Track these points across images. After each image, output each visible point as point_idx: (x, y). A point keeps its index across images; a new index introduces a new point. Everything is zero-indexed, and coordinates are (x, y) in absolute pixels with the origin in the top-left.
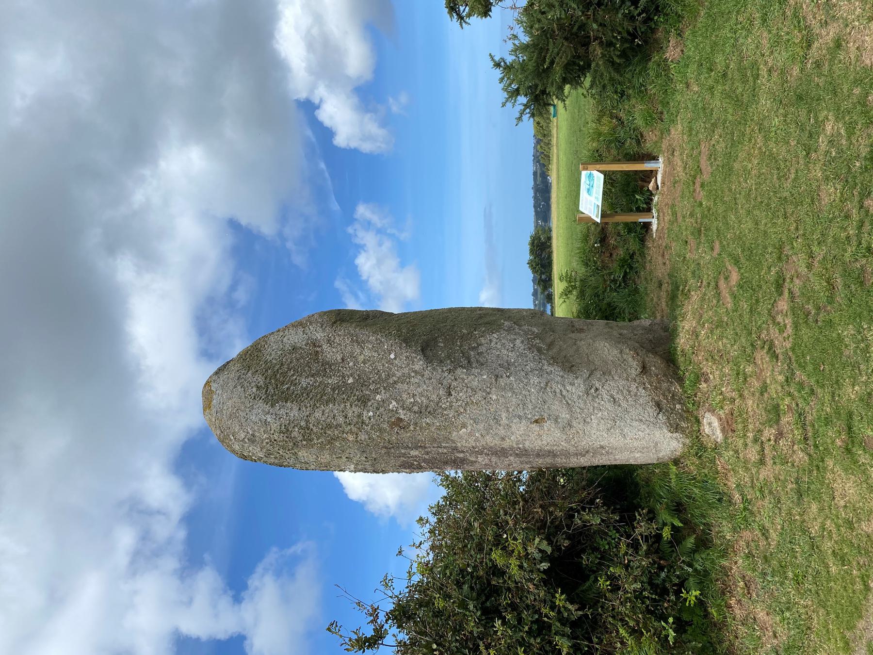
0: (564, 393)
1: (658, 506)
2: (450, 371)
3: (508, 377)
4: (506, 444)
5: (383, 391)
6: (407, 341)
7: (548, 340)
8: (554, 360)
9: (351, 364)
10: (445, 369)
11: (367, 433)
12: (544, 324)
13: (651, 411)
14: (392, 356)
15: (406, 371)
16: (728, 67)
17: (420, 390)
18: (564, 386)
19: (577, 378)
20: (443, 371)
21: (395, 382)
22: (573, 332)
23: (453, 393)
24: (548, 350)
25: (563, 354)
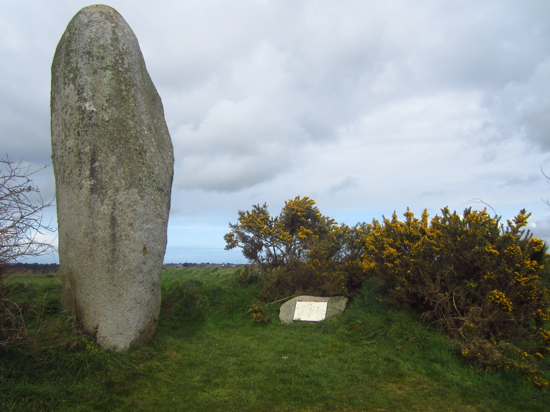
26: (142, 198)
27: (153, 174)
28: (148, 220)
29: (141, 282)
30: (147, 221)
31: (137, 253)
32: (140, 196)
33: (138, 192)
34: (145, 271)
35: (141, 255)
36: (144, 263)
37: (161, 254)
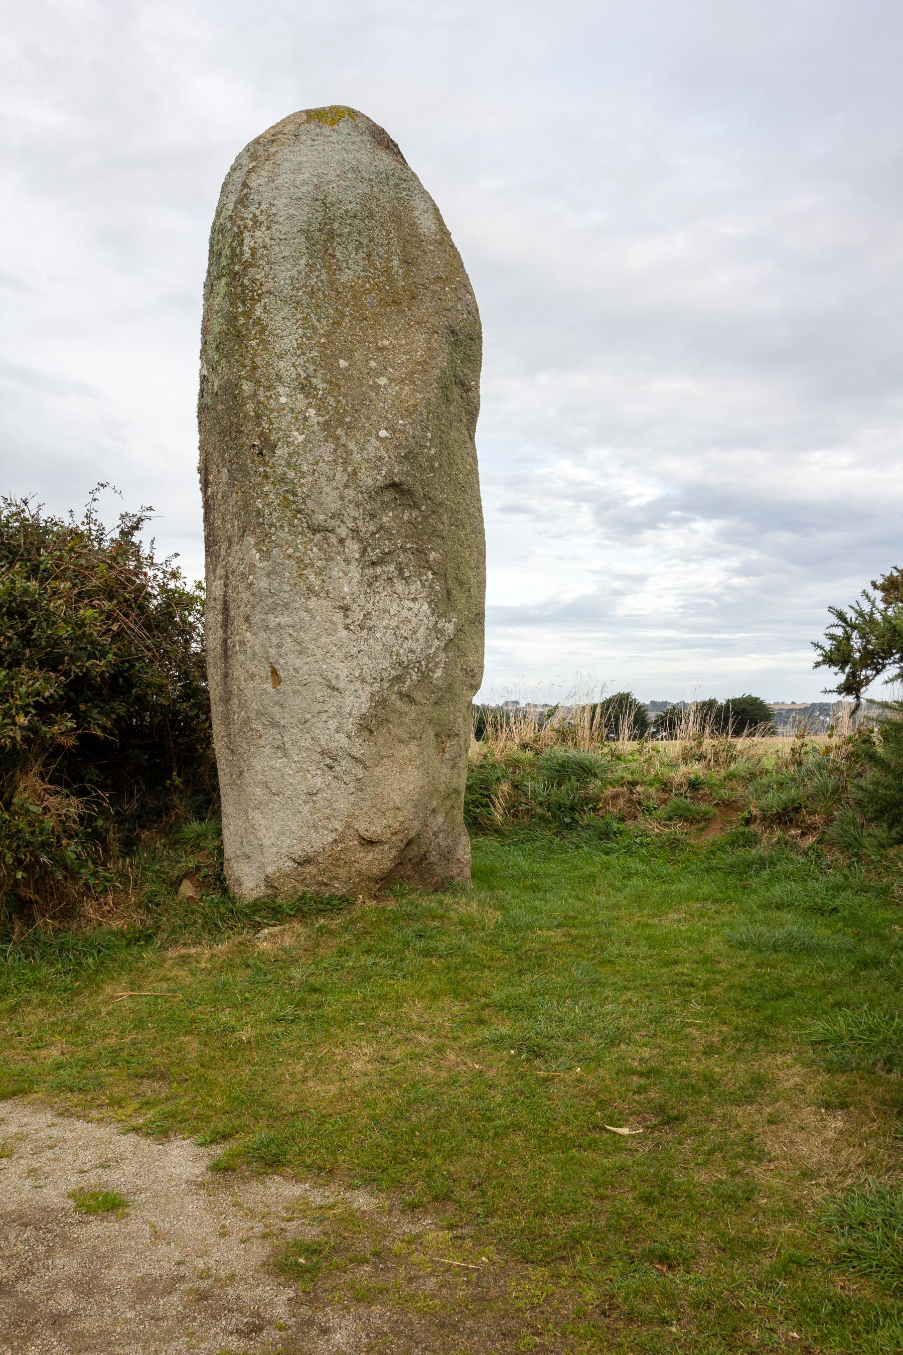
0: (324, 716)
1: (73, 807)
2: (355, 531)
3: (347, 628)
4: (238, 623)
5: (322, 419)
7: (418, 695)
8: (380, 702)
9: (373, 364)
10: (360, 523)
12: (450, 688)
13: (298, 852)
14: (383, 433)
15: (357, 457)
19: (349, 737)
20: (355, 519)
22: (437, 735)
23: (318, 536)
24: (400, 693)
25: (393, 717)
29: (278, 748)
33: (257, 544)
37: (473, 682)
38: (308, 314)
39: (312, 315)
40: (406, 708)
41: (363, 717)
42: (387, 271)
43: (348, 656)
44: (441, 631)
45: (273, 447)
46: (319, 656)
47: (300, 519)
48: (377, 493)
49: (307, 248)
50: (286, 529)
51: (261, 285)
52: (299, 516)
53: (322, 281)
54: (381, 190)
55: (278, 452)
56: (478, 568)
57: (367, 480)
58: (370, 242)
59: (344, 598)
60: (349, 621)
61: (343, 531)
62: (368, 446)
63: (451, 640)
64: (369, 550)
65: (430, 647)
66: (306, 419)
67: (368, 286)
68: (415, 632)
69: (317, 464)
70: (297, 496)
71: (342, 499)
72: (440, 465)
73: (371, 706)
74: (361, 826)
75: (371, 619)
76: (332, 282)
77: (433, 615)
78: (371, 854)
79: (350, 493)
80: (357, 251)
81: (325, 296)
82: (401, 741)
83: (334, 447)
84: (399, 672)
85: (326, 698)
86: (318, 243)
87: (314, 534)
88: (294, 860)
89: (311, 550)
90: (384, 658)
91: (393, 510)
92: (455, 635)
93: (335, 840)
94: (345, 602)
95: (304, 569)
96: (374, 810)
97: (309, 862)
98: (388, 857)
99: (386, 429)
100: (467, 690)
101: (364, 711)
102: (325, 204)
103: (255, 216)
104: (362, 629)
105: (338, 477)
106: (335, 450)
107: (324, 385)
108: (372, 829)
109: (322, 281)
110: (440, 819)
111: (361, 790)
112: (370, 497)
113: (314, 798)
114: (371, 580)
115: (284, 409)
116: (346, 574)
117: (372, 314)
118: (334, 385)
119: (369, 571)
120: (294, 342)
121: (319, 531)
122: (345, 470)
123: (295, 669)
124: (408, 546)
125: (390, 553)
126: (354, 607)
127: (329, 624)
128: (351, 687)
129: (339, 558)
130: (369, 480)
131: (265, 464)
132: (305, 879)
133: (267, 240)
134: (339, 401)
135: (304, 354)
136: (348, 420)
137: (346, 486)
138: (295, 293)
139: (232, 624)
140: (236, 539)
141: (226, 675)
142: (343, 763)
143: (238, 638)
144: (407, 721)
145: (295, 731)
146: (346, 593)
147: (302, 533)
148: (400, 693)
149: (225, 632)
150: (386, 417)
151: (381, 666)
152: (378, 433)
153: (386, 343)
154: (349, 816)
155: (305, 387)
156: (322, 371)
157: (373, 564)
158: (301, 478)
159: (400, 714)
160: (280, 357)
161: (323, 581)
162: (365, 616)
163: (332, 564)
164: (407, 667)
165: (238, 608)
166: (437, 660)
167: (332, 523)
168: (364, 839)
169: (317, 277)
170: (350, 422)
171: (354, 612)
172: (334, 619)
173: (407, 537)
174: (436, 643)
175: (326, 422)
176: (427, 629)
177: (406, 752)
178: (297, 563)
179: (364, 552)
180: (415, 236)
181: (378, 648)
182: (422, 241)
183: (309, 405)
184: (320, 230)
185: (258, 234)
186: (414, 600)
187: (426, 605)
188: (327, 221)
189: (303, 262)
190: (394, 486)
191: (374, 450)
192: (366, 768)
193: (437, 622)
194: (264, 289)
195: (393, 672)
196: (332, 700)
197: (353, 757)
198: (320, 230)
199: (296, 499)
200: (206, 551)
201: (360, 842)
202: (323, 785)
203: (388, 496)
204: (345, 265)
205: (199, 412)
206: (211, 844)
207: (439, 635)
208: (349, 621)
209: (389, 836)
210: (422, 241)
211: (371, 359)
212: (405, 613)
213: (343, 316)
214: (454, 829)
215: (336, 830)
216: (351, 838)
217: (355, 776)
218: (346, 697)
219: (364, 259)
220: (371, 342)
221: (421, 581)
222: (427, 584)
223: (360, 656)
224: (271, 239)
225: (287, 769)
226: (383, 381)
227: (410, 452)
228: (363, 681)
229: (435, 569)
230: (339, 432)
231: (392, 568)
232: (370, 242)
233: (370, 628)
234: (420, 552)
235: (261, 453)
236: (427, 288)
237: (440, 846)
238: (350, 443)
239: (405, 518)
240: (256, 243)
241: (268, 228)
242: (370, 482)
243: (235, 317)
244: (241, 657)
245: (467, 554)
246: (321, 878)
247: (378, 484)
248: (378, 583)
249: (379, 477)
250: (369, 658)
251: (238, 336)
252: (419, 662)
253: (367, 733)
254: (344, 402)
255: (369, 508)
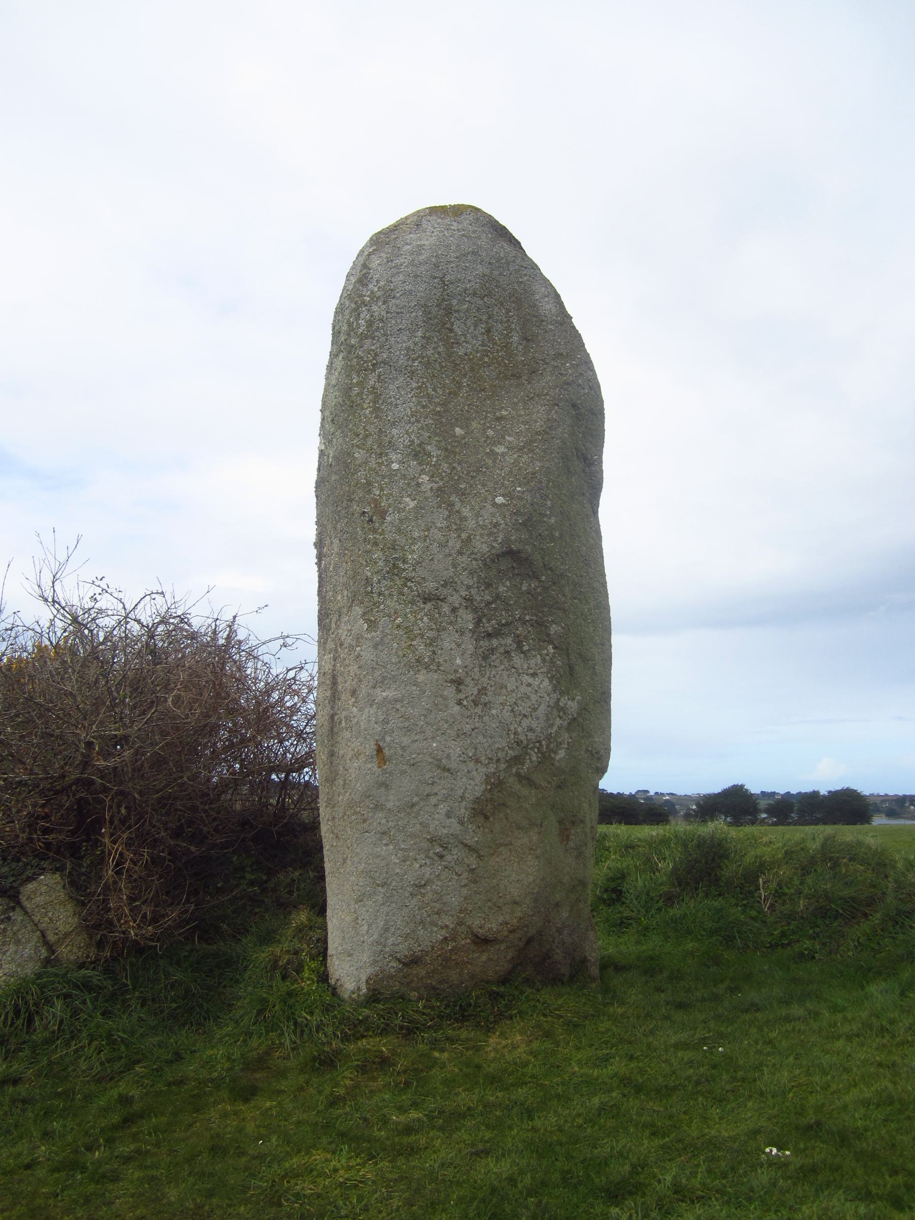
0: (433, 800)
2: (469, 600)
3: (459, 703)
5: (435, 486)
6: (529, 523)
8: (495, 784)
9: (490, 432)
10: (473, 591)
11: (366, 463)
13: (403, 950)
15: (471, 524)
16: (703, 1000)
17: (435, 548)
18: (446, 799)
19: (461, 823)
20: (469, 587)
21: (451, 505)
22: (560, 822)
23: (429, 606)
24: (518, 775)
26: (372, 625)
27: (404, 562)
28: (384, 678)
29: (383, 833)
30: (382, 682)
31: (362, 758)
32: (368, 621)
33: (364, 614)
34: (389, 805)
35: (373, 766)
36: (384, 785)
37: (599, 761)
38: (423, 383)
39: (428, 384)
40: (525, 791)
41: (477, 801)
42: (507, 346)
43: (461, 734)
44: (563, 710)
45: (383, 514)
46: (429, 734)
47: (410, 587)
48: (493, 561)
49: (424, 322)
50: (395, 598)
51: (376, 355)
52: (409, 584)
53: (439, 353)
54: (501, 274)
55: (388, 519)
56: (603, 645)
57: (481, 546)
58: (489, 318)
59: (456, 671)
60: (462, 696)
61: (455, 600)
62: (483, 512)
63: (574, 719)
64: (484, 620)
65: (551, 726)
66: (418, 485)
67: (486, 360)
68: (535, 710)
69: (428, 530)
70: (407, 563)
71: (455, 566)
72: (561, 535)
73: (486, 790)
74: (475, 922)
75: (486, 694)
76: (450, 355)
77: (555, 691)
78: (486, 954)
79: (464, 560)
80: (476, 326)
81: (442, 367)
82: (519, 828)
83: (447, 513)
84: (517, 753)
85: (436, 780)
86: (435, 317)
87: (424, 603)
88: (399, 960)
89: (421, 619)
90: (501, 737)
91: (509, 579)
92: (578, 714)
93: (446, 939)
94: (458, 675)
95: (412, 640)
96: (489, 904)
97: (416, 963)
98: (505, 957)
99: (503, 496)
100: (592, 773)
101: (478, 794)
102: (443, 282)
103: (372, 292)
104: (476, 705)
105: (450, 544)
106: (449, 516)
107: (439, 452)
108: (488, 926)
109: (439, 353)
110: (565, 914)
111: (475, 882)
112: (485, 564)
113: (422, 891)
114: (486, 652)
115: (396, 475)
116: (459, 646)
117: (491, 386)
118: (448, 453)
119: (485, 643)
120: (408, 410)
121: (430, 600)
122: (459, 536)
123: (403, 748)
124: (527, 618)
125: (507, 624)
126: (468, 680)
127: (440, 699)
128: (464, 768)
129: (451, 628)
130: (484, 546)
131: (375, 531)
132: (412, 981)
133: (383, 313)
134: (454, 468)
135: (418, 421)
136: (463, 486)
137: (460, 553)
138: (410, 363)
139: (339, 699)
140: (345, 610)
141: (332, 754)
142: (454, 852)
143: (344, 713)
144: (527, 806)
145: (402, 815)
146: (458, 666)
147: (413, 603)
148: (518, 775)
149: (332, 708)
150: (503, 484)
151: (497, 746)
152: (494, 499)
153: (504, 413)
154: (461, 911)
155: (418, 453)
156: (437, 438)
157: (489, 636)
158: (412, 544)
159: (519, 798)
160: (394, 424)
161: (434, 653)
162: (479, 691)
163: (444, 635)
164: (526, 747)
165: (346, 682)
166: (560, 740)
167: (445, 592)
168: (477, 937)
169: (434, 348)
170: (465, 489)
171: (467, 686)
172: (445, 693)
173: (525, 608)
174: (558, 722)
175: (439, 489)
176: (548, 706)
177: (526, 840)
178: (406, 633)
179: (478, 622)
180: (535, 316)
181: (494, 726)
182: (543, 321)
183: (423, 472)
184: (438, 306)
185: (375, 308)
186: (534, 675)
187: (547, 680)
188: (446, 297)
189: (420, 334)
190: (510, 553)
191: (487, 516)
192: (480, 857)
193: (558, 700)
194: (379, 359)
195: (510, 752)
196: (443, 782)
197: (466, 845)
198: (438, 306)
199: (406, 566)
200: (319, 625)
201: (473, 941)
202: (433, 876)
203: (505, 564)
204: (463, 339)
205: (316, 487)
206: (316, 935)
207: (561, 714)
208: (462, 696)
209: (506, 933)
210: (543, 321)
211: (488, 428)
212: (523, 689)
213: (460, 387)
214: (579, 924)
215: (447, 926)
216: (463, 936)
217: (468, 866)
218: (458, 778)
219: (482, 334)
220: (489, 412)
221: (541, 655)
222: (548, 658)
223: (474, 734)
224: (387, 313)
225: (393, 857)
226: (500, 449)
227: (529, 519)
228: (477, 761)
229: (556, 642)
230: (453, 498)
231: (509, 641)
232: (489, 318)
233: (485, 704)
234: (540, 625)
235: (371, 520)
236: (547, 364)
237: (564, 943)
238: (464, 510)
239: (524, 588)
240: (372, 316)
241: (384, 303)
242: (485, 548)
243: (350, 388)
244: (347, 734)
245: (591, 629)
246: (429, 981)
247: (494, 551)
248: (495, 657)
249: (495, 544)
250: (485, 737)
251: (352, 406)
252: (540, 742)
253: (481, 819)
254: (459, 469)
255: (483, 575)
